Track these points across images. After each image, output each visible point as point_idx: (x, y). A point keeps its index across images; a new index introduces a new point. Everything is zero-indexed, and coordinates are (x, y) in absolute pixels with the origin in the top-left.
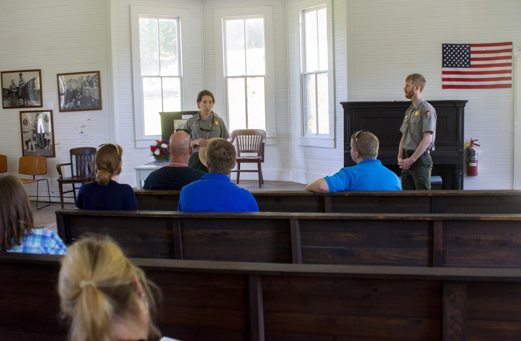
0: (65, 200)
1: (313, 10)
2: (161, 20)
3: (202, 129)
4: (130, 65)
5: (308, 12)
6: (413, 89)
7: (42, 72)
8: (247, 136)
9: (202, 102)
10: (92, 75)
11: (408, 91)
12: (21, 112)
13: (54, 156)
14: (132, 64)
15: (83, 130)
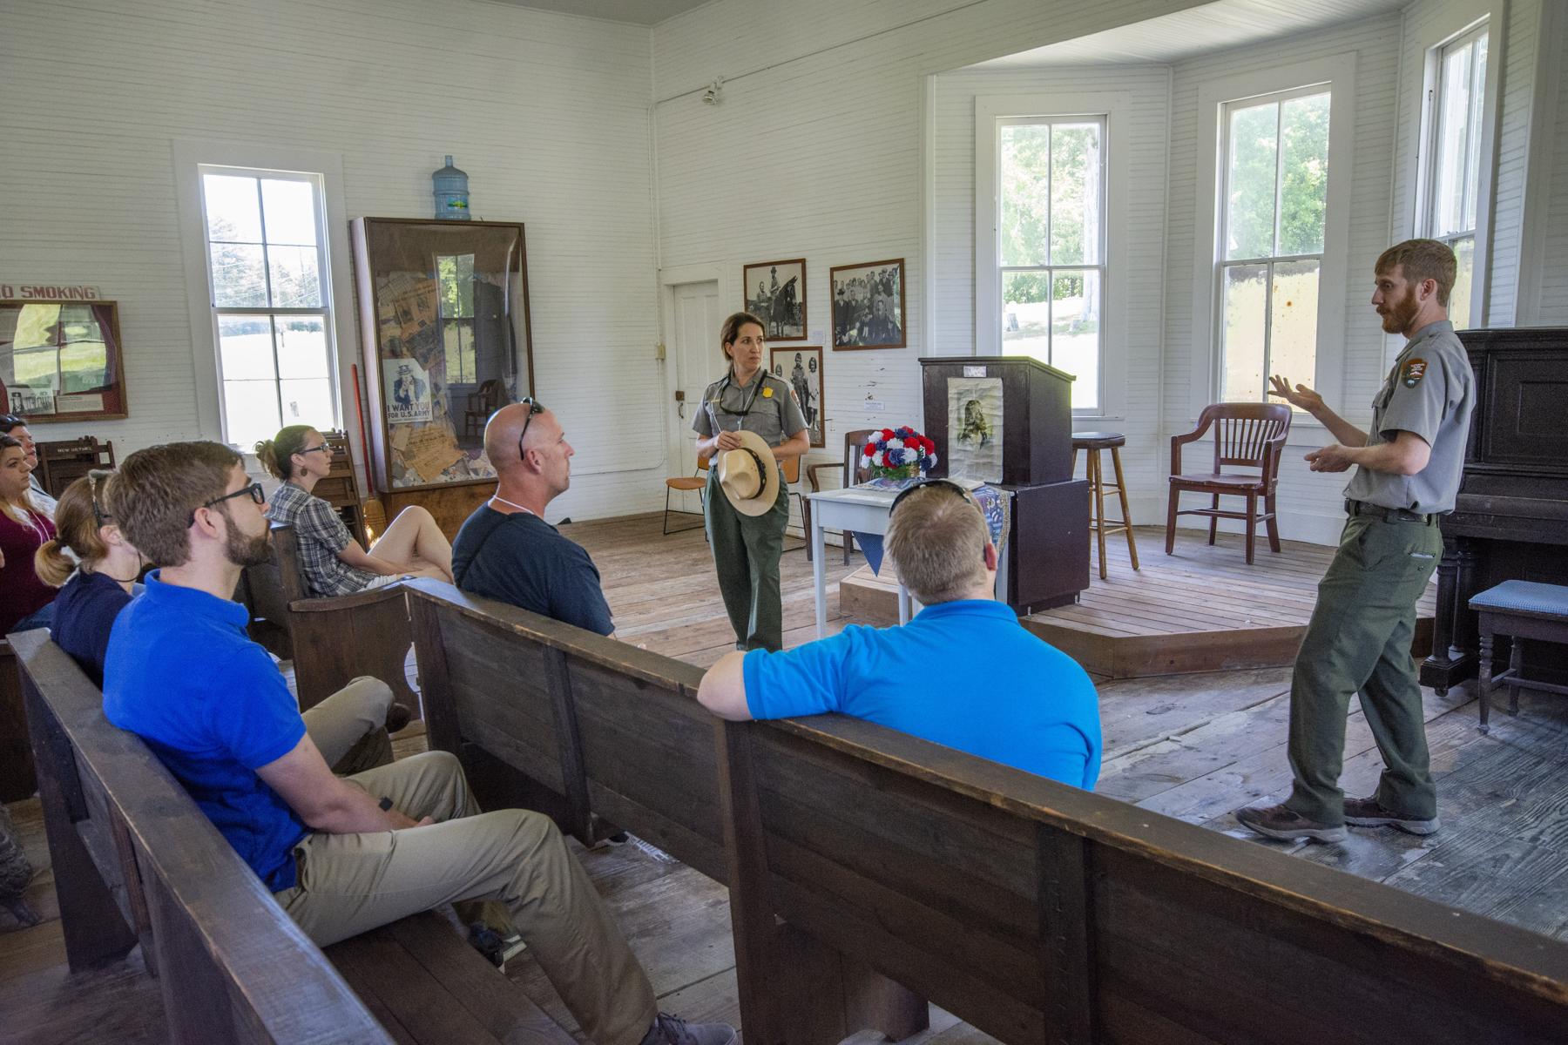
0: (1204, 523)
1: (1461, 46)
2: (1059, 128)
3: (728, 412)
4: (969, 244)
5: (1453, 50)
6: (1410, 293)
7: (808, 265)
8: (1240, 421)
9: (737, 343)
10: (889, 268)
11: (1392, 305)
12: (773, 350)
13: (822, 445)
14: (974, 240)
15: (873, 391)
